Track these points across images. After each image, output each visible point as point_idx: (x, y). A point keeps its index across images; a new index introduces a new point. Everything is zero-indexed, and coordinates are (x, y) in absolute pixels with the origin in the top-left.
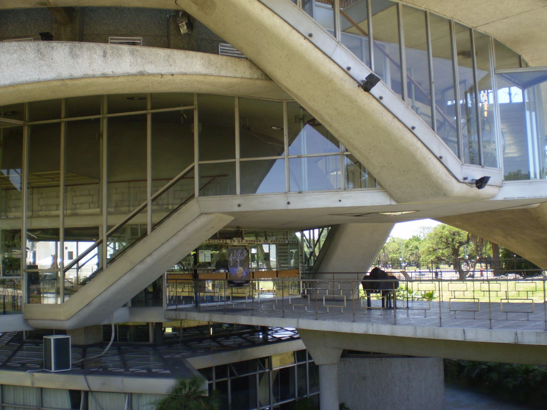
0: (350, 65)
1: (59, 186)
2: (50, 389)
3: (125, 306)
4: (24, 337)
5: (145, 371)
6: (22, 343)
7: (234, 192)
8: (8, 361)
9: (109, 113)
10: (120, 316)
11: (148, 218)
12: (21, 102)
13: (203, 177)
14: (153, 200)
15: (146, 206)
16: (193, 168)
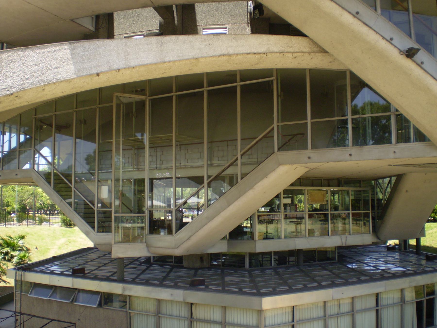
0: (392, 36)
3: (224, 238)
4: (152, 261)
5: (237, 290)
6: (151, 265)
8: (137, 278)
10: (222, 248)
13: (245, 139)
14: (242, 155)
15: (237, 160)
16: (273, 129)
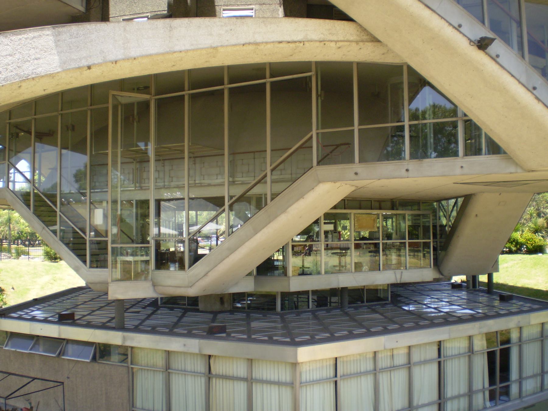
0: (461, 22)
1: (224, 155)
2: (178, 352)
4: (159, 303)
5: (266, 338)
7: (352, 161)
8: (140, 324)
9: (230, 84)
10: (247, 286)
11: (266, 189)
12: (221, 65)
14: (272, 170)
15: (265, 176)
16: (311, 137)
